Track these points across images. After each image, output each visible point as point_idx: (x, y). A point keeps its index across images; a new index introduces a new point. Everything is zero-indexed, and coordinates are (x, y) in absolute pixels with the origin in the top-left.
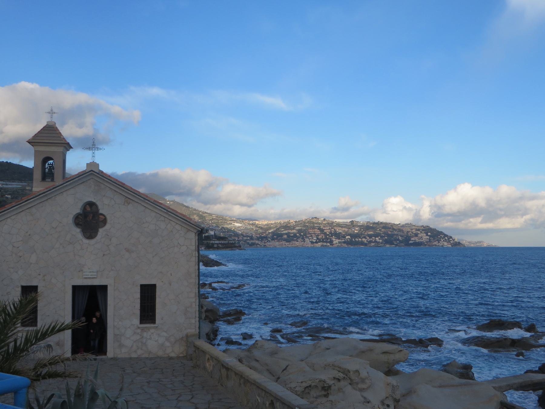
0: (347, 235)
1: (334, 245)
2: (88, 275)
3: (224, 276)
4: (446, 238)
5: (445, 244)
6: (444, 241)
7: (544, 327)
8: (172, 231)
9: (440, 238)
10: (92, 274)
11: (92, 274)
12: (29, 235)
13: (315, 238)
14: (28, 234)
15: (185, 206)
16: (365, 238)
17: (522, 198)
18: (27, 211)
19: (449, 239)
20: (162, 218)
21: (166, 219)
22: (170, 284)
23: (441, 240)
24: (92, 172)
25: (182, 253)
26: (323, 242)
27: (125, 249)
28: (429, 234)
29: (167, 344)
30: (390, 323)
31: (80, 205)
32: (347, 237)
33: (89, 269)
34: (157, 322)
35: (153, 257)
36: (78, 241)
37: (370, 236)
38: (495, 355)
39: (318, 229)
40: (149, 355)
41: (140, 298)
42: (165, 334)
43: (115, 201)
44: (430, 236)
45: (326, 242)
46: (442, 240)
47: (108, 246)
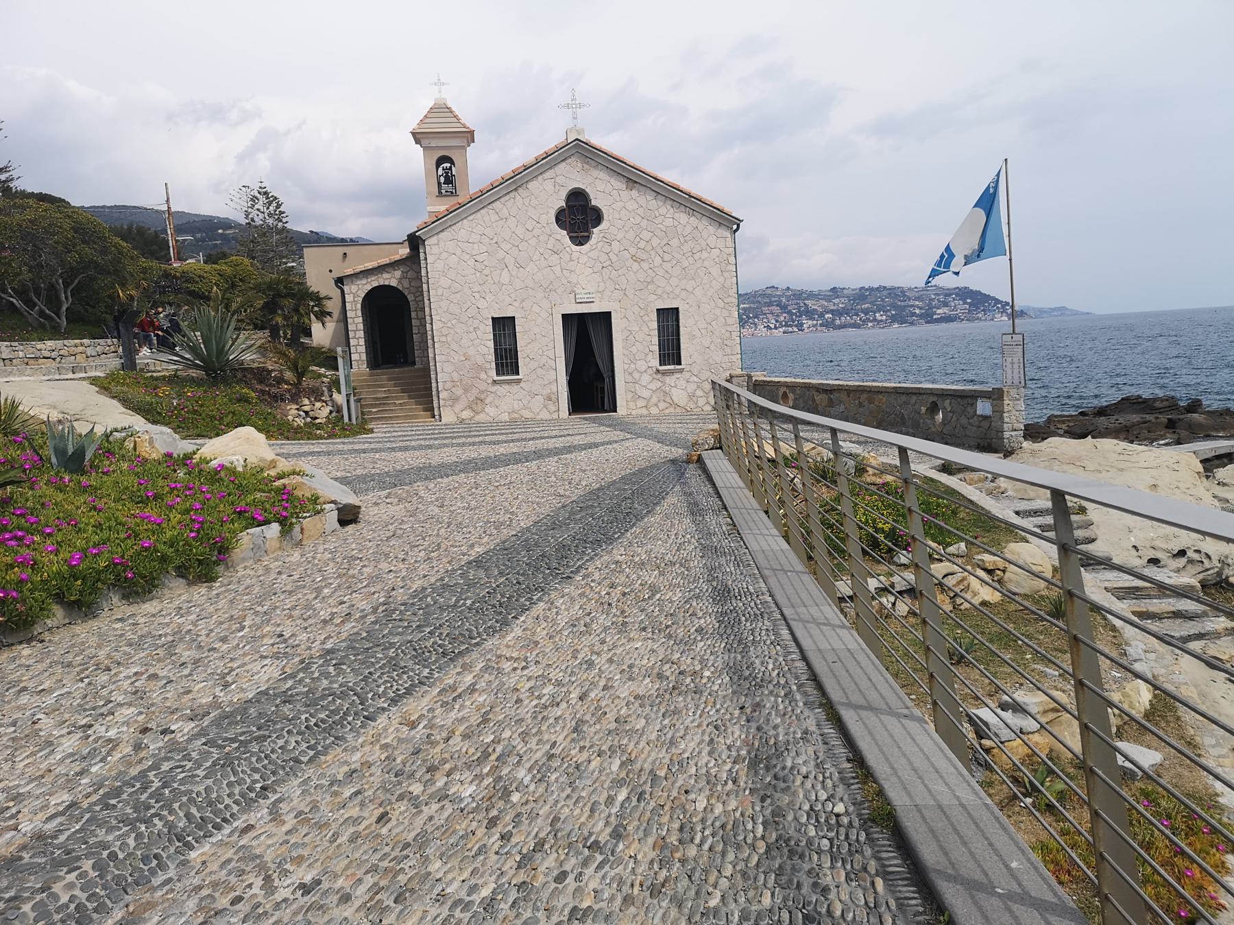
0: (827, 313)
1: (425, 770)
3: (275, 723)
7: (1232, 511)
13: (773, 321)
14: (494, 241)
16: (857, 315)
17: (939, 871)
18: (490, 207)
19: (1003, 306)
26: (786, 325)
28: (969, 301)
31: (563, 194)
32: (827, 316)
34: (683, 363)
37: (866, 312)
39: (777, 305)
42: (696, 379)
44: (970, 304)
45: (791, 326)
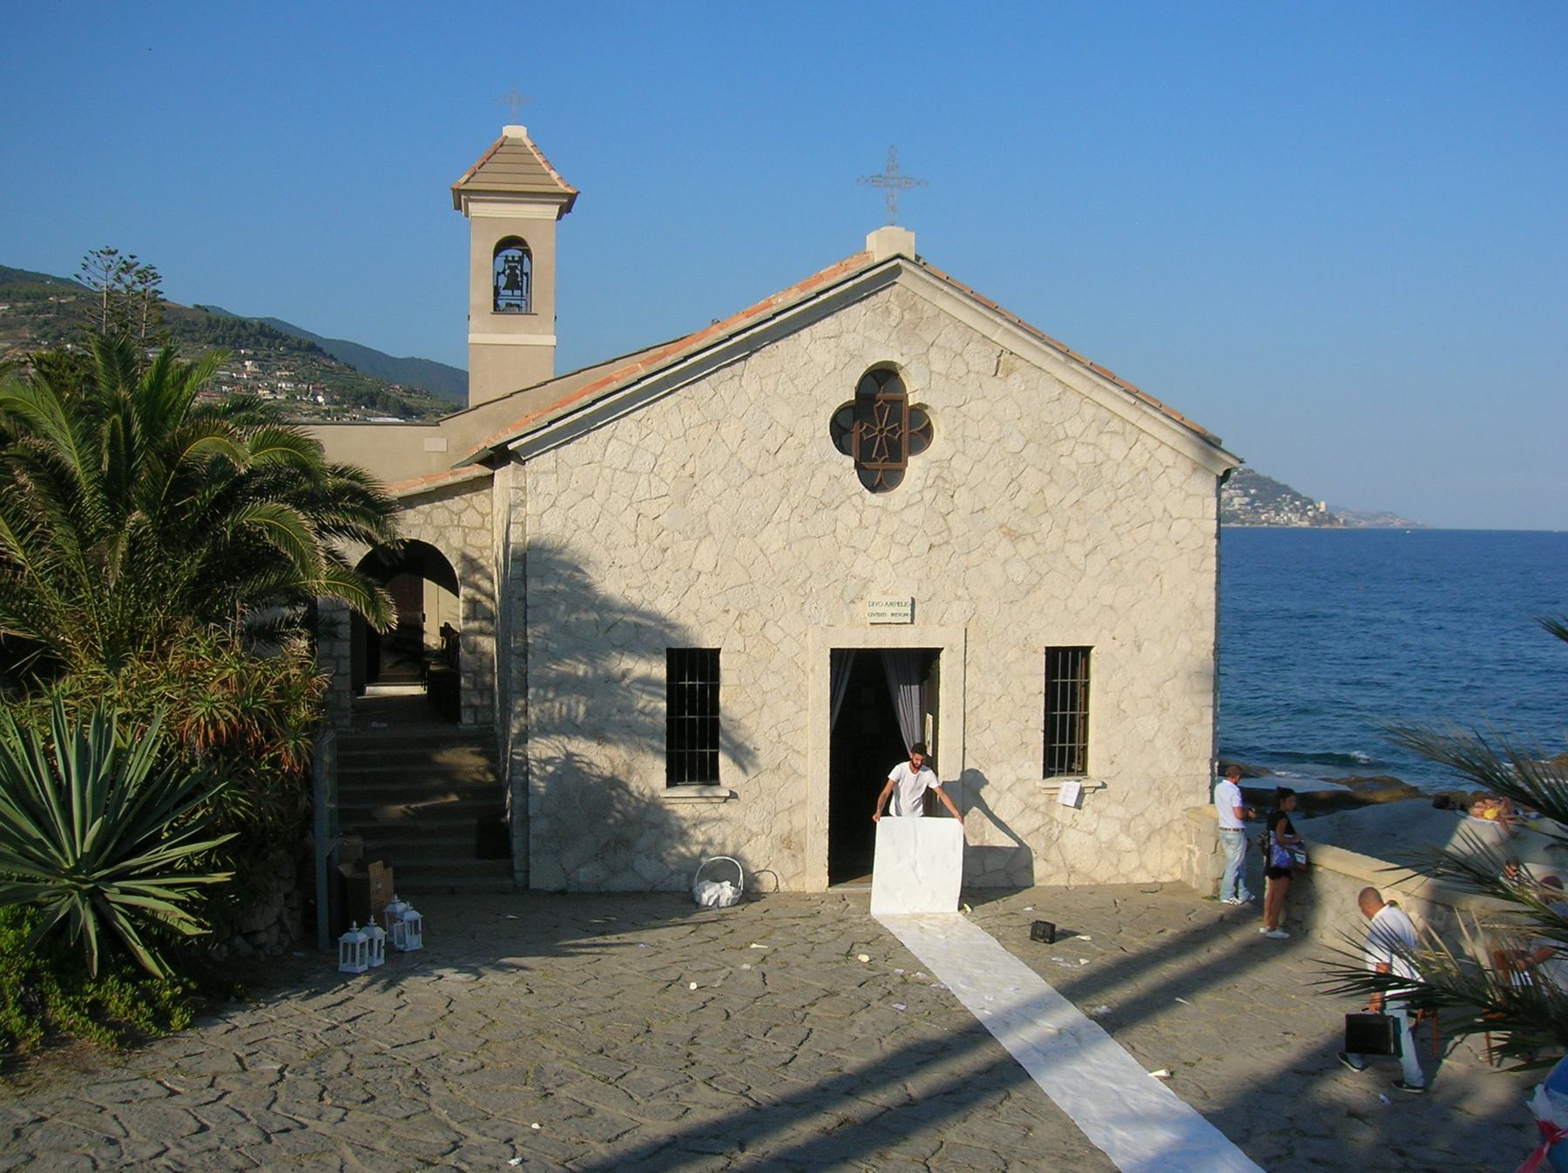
2: (884, 614)
4: (1297, 503)
5: (1294, 518)
6: (1291, 510)
8: (1146, 469)
9: (1280, 503)
10: (895, 609)
11: (895, 609)
12: (692, 476)
15: (876, 379)
19: (1304, 505)
20: (1115, 425)
21: (1129, 427)
22: (1139, 648)
23: (1282, 509)
24: (899, 261)
25: (1177, 543)
27: (1001, 527)
29: (1126, 842)
30: (221, 732)
33: (884, 593)
35: (1086, 556)
36: (849, 497)
38: (1492, 867)
40: (1069, 880)
41: (1044, 691)
42: (1119, 811)
43: (967, 364)
46: (1286, 509)
47: (945, 516)
